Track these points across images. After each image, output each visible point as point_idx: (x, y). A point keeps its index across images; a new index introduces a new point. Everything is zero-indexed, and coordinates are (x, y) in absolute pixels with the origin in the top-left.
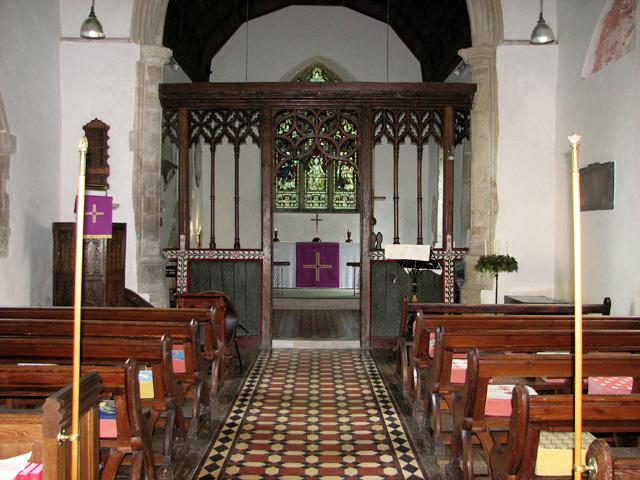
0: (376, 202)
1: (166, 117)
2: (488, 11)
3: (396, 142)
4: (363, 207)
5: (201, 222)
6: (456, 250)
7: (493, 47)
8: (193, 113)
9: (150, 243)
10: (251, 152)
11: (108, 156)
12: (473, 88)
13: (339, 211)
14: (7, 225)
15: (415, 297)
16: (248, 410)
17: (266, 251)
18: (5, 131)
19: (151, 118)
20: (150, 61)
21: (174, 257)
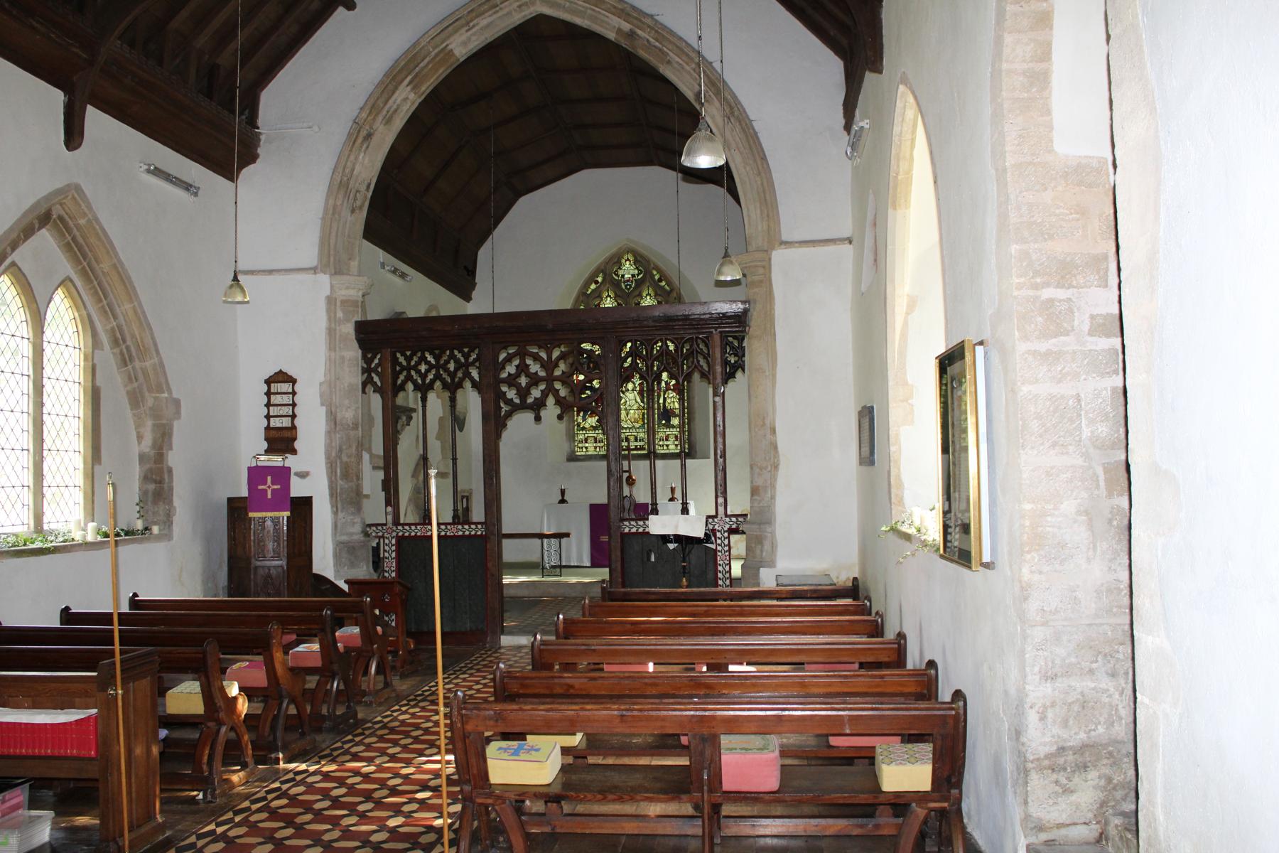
2: (761, 203)
7: (767, 253)
8: (398, 355)
9: (350, 518)
14: (170, 502)
18: (166, 395)
19: (346, 363)
20: (343, 293)
21: (380, 534)
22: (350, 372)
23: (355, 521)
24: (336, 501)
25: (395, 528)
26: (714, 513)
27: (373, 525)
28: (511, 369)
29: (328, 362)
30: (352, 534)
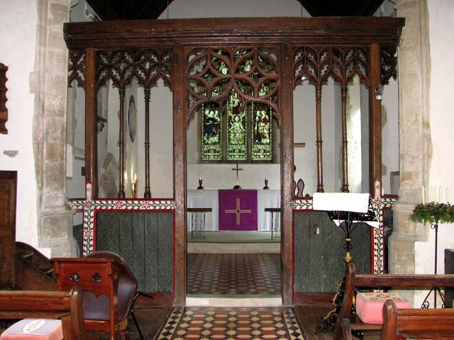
0: (296, 149)
1: (71, 57)
3: (318, 83)
4: (280, 155)
5: (136, 171)
6: (385, 197)
10: (162, 95)
11: (7, 100)
12: (401, 22)
13: (257, 162)
15: (348, 254)
16: (182, 317)
17: (179, 199)
19: (55, 58)
21: (81, 207)
22: (58, 66)
23: (59, 195)
24: (42, 178)
25: (93, 202)
26: (172, 197)
27: (74, 199)
28: (198, 68)
29: (38, 55)
30: (55, 207)
